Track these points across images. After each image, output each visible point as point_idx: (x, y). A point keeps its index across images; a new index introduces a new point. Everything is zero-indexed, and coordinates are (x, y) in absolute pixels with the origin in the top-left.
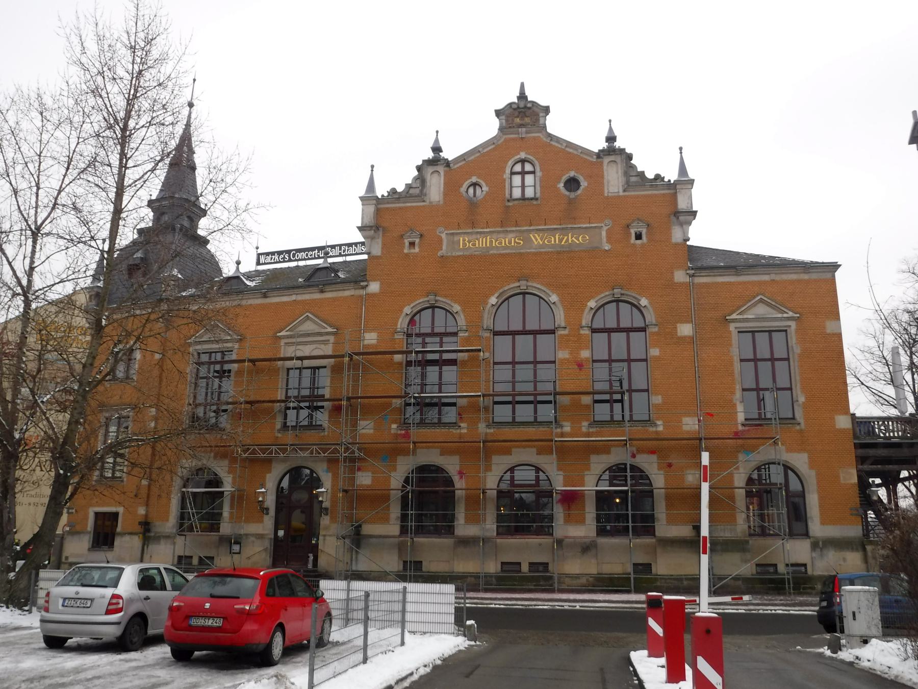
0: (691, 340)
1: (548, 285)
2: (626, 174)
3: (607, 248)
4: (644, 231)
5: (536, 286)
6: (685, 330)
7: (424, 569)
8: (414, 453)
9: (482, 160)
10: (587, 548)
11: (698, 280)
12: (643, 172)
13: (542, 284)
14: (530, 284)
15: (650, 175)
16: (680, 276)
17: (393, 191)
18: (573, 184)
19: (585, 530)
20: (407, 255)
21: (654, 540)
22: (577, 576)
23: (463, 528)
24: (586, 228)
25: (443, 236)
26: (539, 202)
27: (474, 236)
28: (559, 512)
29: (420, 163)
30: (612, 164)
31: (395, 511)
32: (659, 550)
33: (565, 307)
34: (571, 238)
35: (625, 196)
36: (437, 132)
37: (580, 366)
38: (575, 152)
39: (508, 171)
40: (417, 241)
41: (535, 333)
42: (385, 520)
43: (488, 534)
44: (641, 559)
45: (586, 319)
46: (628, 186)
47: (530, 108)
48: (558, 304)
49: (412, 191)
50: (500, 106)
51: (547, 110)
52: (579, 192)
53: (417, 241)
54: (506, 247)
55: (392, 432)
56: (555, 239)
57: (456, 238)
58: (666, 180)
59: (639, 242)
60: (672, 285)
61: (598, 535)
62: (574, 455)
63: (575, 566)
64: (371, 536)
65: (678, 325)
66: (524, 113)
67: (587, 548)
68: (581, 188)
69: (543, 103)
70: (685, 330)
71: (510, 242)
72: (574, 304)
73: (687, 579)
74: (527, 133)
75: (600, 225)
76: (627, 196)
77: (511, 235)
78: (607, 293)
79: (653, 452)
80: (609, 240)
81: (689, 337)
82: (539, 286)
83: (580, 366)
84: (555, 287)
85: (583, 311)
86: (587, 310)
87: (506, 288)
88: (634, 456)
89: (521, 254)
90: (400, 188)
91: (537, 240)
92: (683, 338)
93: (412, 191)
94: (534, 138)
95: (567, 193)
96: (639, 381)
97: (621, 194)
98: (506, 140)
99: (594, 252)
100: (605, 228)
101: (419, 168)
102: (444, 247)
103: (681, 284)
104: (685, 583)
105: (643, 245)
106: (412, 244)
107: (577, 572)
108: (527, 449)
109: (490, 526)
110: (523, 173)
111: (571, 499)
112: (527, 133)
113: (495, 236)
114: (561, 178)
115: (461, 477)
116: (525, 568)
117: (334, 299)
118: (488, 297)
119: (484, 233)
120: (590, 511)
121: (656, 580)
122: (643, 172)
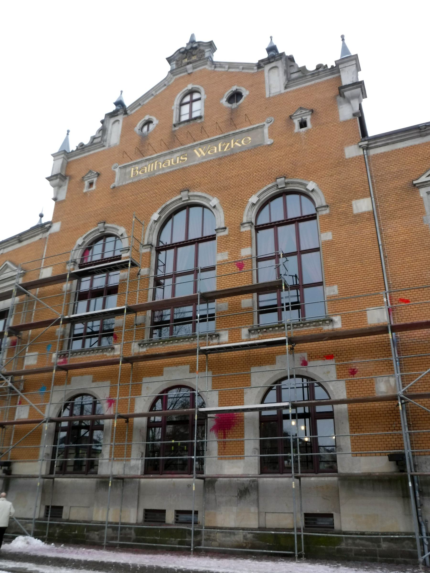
0: (371, 216)
1: (208, 191)
2: (287, 73)
3: (269, 143)
4: (308, 119)
5: (197, 195)
6: (363, 205)
7: (64, 517)
8: (69, 382)
9: (155, 99)
10: (245, 491)
11: (372, 152)
12: (304, 67)
13: (202, 191)
14: (191, 193)
15: (311, 68)
16: (352, 151)
17: (82, 145)
18: (236, 96)
19: (243, 465)
20: (86, 194)
21: (336, 479)
22: (232, 531)
23: (107, 466)
24: (248, 130)
25: (117, 170)
26: (203, 120)
27: (143, 164)
28: (213, 443)
29: (103, 118)
30: (273, 70)
31: (45, 447)
32: (342, 494)
33: (223, 208)
34: (234, 144)
35: (287, 93)
36: (122, 92)
37: (240, 266)
38: (237, 70)
39: (177, 102)
40: (95, 180)
41: (197, 242)
42: (33, 457)
43: (133, 473)
44: (316, 506)
45: (248, 215)
46: (289, 82)
47: (196, 48)
48: (219, 207)
49: (95, 141)
50: (170, 53)
51: (211, 45)
52: (241, 101)
53: (95, 180)
54: (172, 166)
55: (53, 361)
56: (218, 149)
57: (128, 170)
58: (329, 67)
59: (303, 129)
60: (343, 162)
61: (262, 471)
62: (229, 365)
63: (230, 516)
64: (20, 477)
65: (354, 202)
66: (191, 53)
67: (245, 491)
68: (243, 97)
69: (206, 39)
70: (363, 205)
71: (175, 162)
72: (233, 204)
73: (385, 540)
74: (194, 68)
75: (262, 124)
76: (289, 92)
77: (176, 155)
78: (270, 185)
79: (329, 357)
80: (271, 135)
81: (369, 212)
82: (200, 194)
83: (240, 266)
84: (214, 192)
85: (244, 208)
86: (248, 206)
87: (168, 203)
88: (305, 364)
89: (183, 169)
90: (86, 142)
91: (200, 153)
92: (361, 215)
93: (95, 141)
94: (201, 71)
95: (230, 105)
96: (312, 274)
97: (283, 91)
98: (175, 80)
99: (256, 149)
100: (267, 126)
101: (102, 122)
102: (117, 179)
103: (353, 159)
104: (384, 546)
105: (308, 131)
106: (91, 184)
107: (232, 524)
108: (180, 367)
109: (136, 464)
110: (192, 101)
111: (228, 423)
112: (194, 68)
113: (162, 159)
114: (224, 95)
115: (110, 405)
116: (170, 518)
117: (28, 245)
118: (151, 214)
119: (152, 159)
120: (251, 441)
121: (340, 540)
122: (304, 67)
